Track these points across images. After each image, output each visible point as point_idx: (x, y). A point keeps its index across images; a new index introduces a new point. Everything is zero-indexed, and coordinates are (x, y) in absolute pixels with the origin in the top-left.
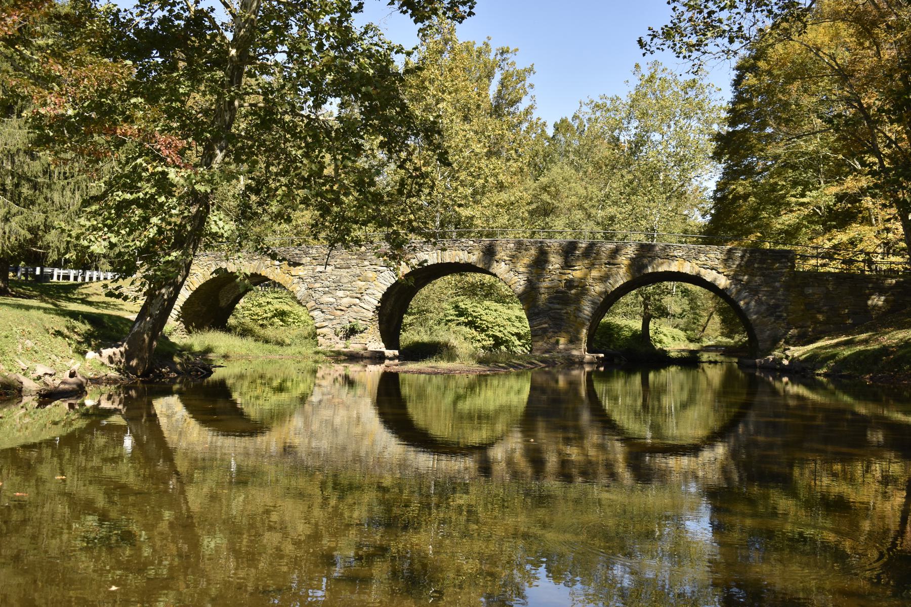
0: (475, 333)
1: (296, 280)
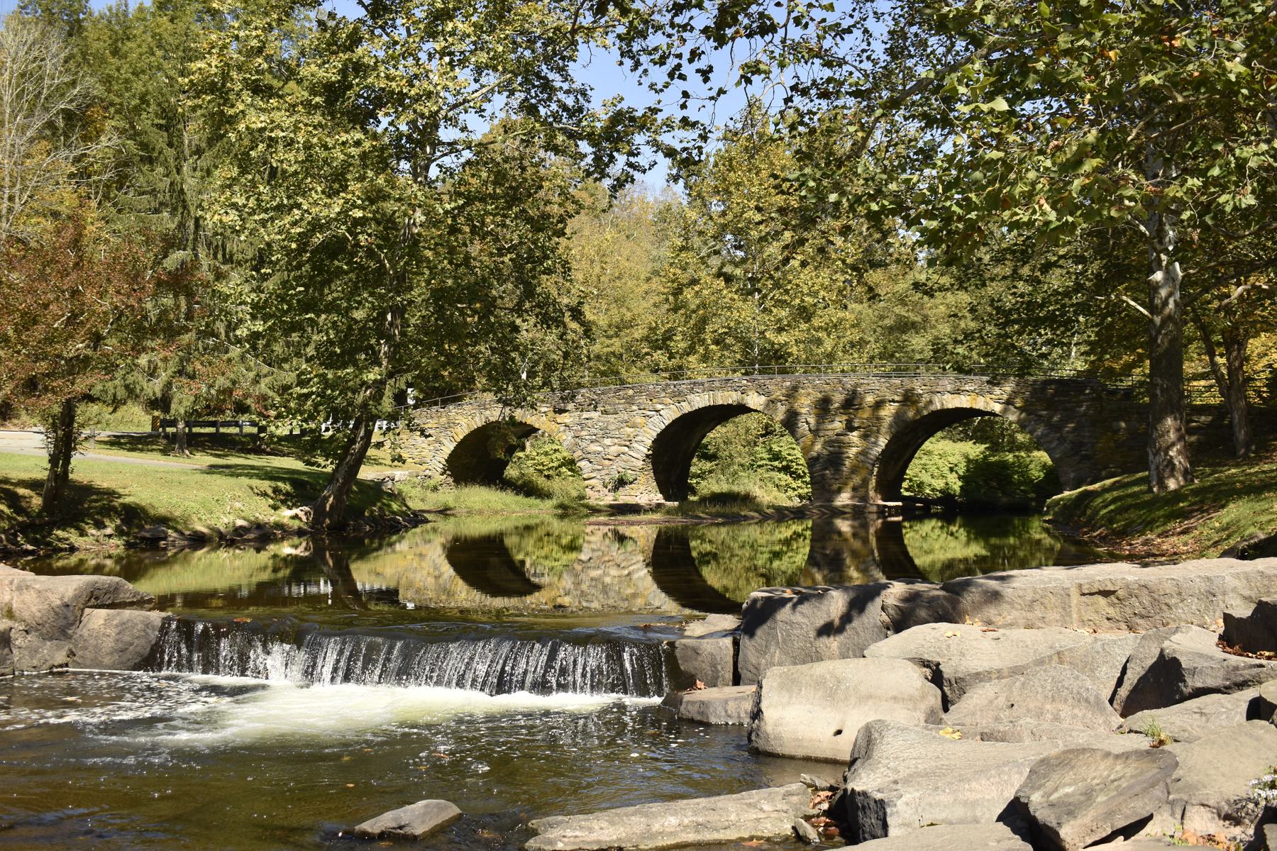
0: (790, 480)
1: (562, 428)
